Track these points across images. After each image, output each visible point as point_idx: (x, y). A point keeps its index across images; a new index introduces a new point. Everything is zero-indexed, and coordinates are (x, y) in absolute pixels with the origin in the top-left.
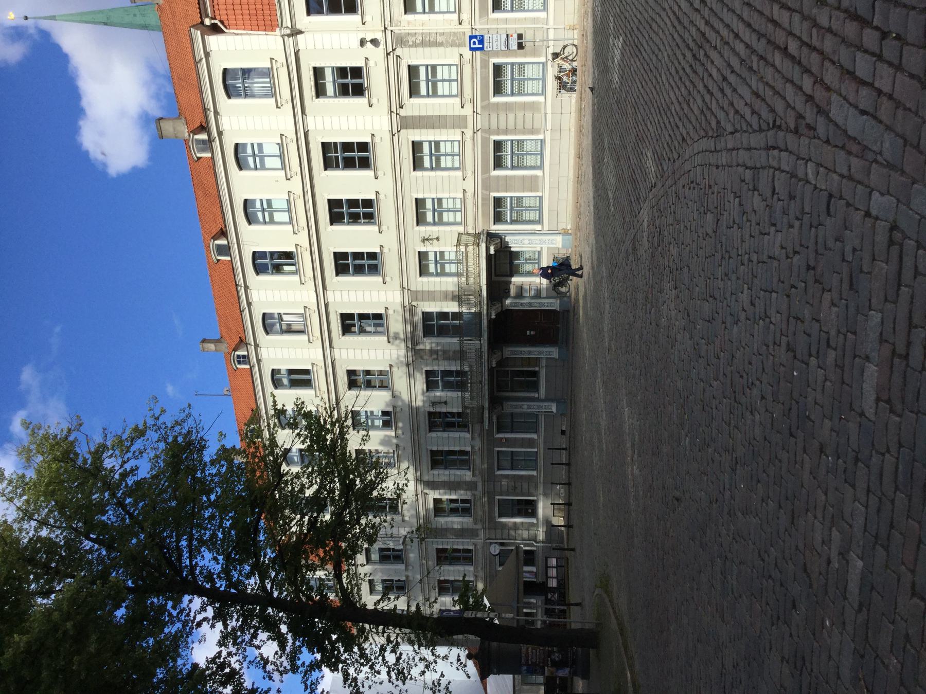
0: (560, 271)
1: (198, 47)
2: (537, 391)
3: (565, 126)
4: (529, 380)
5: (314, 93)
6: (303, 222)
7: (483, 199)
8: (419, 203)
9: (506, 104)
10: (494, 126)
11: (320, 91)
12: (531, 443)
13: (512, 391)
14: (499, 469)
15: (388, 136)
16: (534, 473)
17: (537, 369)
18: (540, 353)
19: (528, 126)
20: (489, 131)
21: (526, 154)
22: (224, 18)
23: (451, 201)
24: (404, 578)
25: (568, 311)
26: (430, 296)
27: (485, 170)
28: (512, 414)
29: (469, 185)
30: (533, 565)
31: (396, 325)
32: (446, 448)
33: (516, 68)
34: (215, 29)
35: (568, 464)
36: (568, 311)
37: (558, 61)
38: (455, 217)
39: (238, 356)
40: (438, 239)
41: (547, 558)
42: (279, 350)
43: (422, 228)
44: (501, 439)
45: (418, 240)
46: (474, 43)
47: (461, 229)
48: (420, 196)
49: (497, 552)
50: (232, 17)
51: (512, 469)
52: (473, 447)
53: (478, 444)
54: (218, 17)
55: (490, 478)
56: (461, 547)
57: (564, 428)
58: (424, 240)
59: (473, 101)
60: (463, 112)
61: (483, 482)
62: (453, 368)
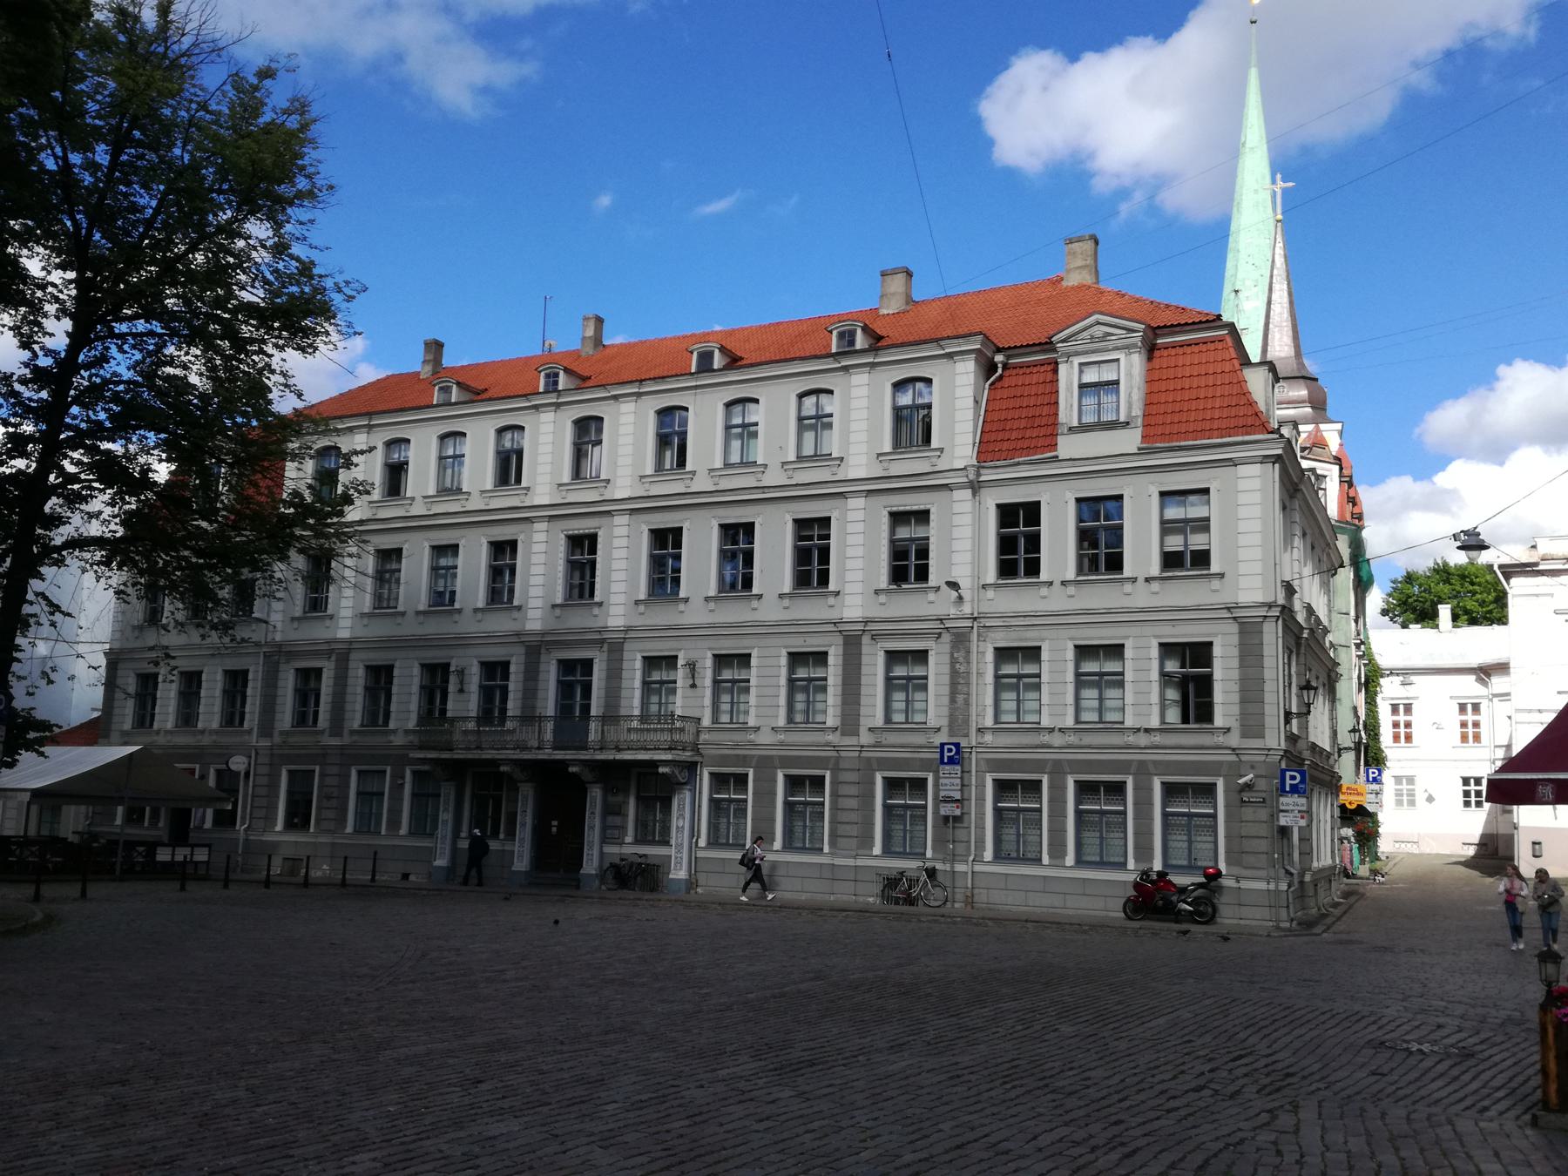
0: (638, 878)
3: (1245, 911)
6: (725, 484)
7: (745, 756)
8: (744, 660)
11: (898, 518)
12: (394, 823)
13: (473, 796)
14: (360, 773)
15: (833, 615)
16: (349, 829)
17: (502, 836)
18: (522, 840)
20: (835, 771)
21: (1101, 838)
22: (1006, 382)
23: (1035, 705)
25: (578, 887)
26: (615, 674)
27: (786, 762)
28: (439, 795)
29: (765, 737)
31: (578, 620)
32: (395, 690)
33: (1208, 822)
34: (989, 368)
35: (344, 883)
36: (578, 887)
37: (924, 876)
38: (899, 711)
39: (557, 375)
40: (693, 686)
41: (209, 846)
42: (550, 438)
43: (709, 662)
44: (403, 777)
45: (693, 655)
46: (950, 750)
47: (706, 722)
48: (754, 662)
49: (233, 767)
50: (1006, 393)
51: (359, 794)
52: (394, 732)
53: (398, 740)
54: (1007, 373)
55: (348, 756)
56: (247, 709)
57: (412, 878)
59: (878, 745)
60: (863, 731)
61: (342, 747)
62: (510, 705)
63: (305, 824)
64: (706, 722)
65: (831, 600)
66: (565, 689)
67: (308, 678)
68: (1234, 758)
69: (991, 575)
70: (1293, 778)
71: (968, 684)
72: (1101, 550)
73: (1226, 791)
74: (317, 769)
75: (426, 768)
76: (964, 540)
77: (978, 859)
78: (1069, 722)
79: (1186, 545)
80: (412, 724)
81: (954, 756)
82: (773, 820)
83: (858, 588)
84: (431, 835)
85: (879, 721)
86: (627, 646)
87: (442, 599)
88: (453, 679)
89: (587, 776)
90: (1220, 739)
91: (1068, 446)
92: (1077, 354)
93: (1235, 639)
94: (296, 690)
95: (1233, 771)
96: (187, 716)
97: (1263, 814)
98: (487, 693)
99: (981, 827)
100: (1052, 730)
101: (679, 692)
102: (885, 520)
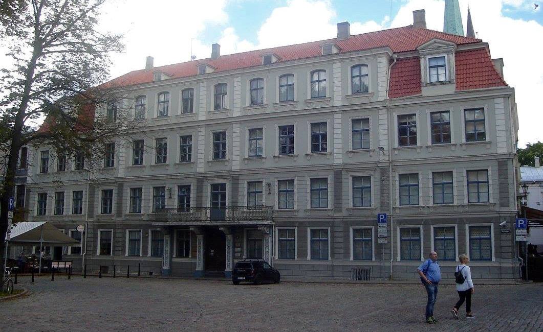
1: (378, 51)
2: (177, 257)
4: (183, 251)
5: (314, 122)
9: (349, 236)
10: (336, 229)
11: (355, 121)
12: (145, 252)
13: (177, 240)
14: (130, 231)
16: (127, 254)
17: (190, 256)
19: (336, 251)
20: (333, 226)
24: (144, 164)
26: (235, 189)
27: (311, 224)
28: (163, 240)
29: (301, 215)
30: (72, 252)
40: (270, 193)
43: (276, 184)
45: (269, 181)
46: (382, 217)
47: (276, 208)
48: (296, 183)
51: (130, 240)
53: (145, 218)
55: (125, 226)
57: (153, 274)
58: (269, 185)
62: (191, 203)
63: (109, 253)
64: (276, 208)
65: (328, 157)
66: (214, 196)
67: (107, 194)
68: (498, 215)
69: (396, 145)
70: (521, 222)
71: (389, 189)
72: (441, 134)
73: (495, 228)
74: (112, 230)
75: (159, 229)
76: (384, 132)
77: (395, 259)
78: (466, 202)
79: (475, 131)
80: (150, 212)
81: (385, 219)
82: (306, 248)
83: (203, 161)
84: (161, 256)
85: (351, 206)
86: (240, 178)
87: (255, 155)
88: (167, 193)
89: (226, 231)
90: (492, 208)
91: (425, 92)
92: (428, 54)
93: (496, 168)
94: (102, 199)
95: (497, 220)
96: (59, 211)
97: (509, 237)
98: (181, 199)
99: (395, 248)
100: (423, 207)
101: (264, 197)
102: (350, 123)
